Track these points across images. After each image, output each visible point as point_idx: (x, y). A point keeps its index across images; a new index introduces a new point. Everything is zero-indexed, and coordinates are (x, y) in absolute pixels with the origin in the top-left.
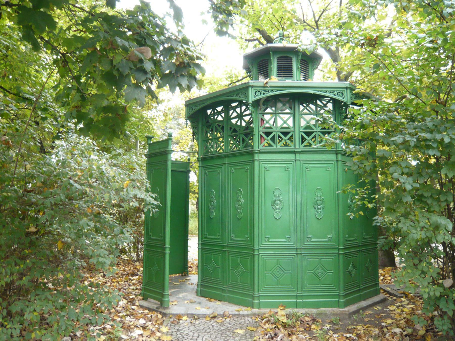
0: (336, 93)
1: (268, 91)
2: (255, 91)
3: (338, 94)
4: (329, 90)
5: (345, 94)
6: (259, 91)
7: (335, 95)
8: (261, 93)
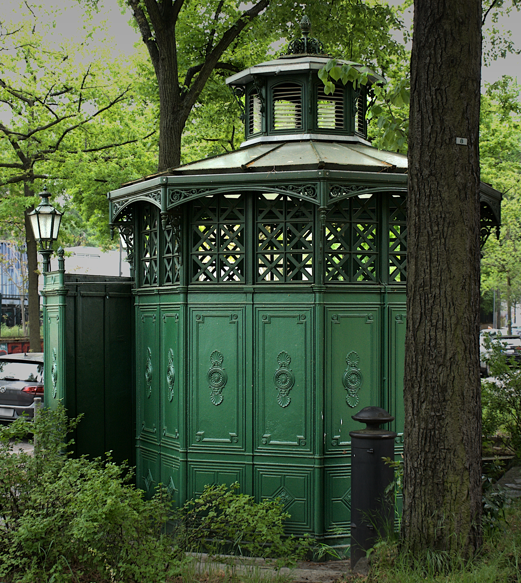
1: (192, 192)
2: (171, 192)
4: (291, 185)
5: (318, 191)
6: (178, 192)
8: (180, 196)
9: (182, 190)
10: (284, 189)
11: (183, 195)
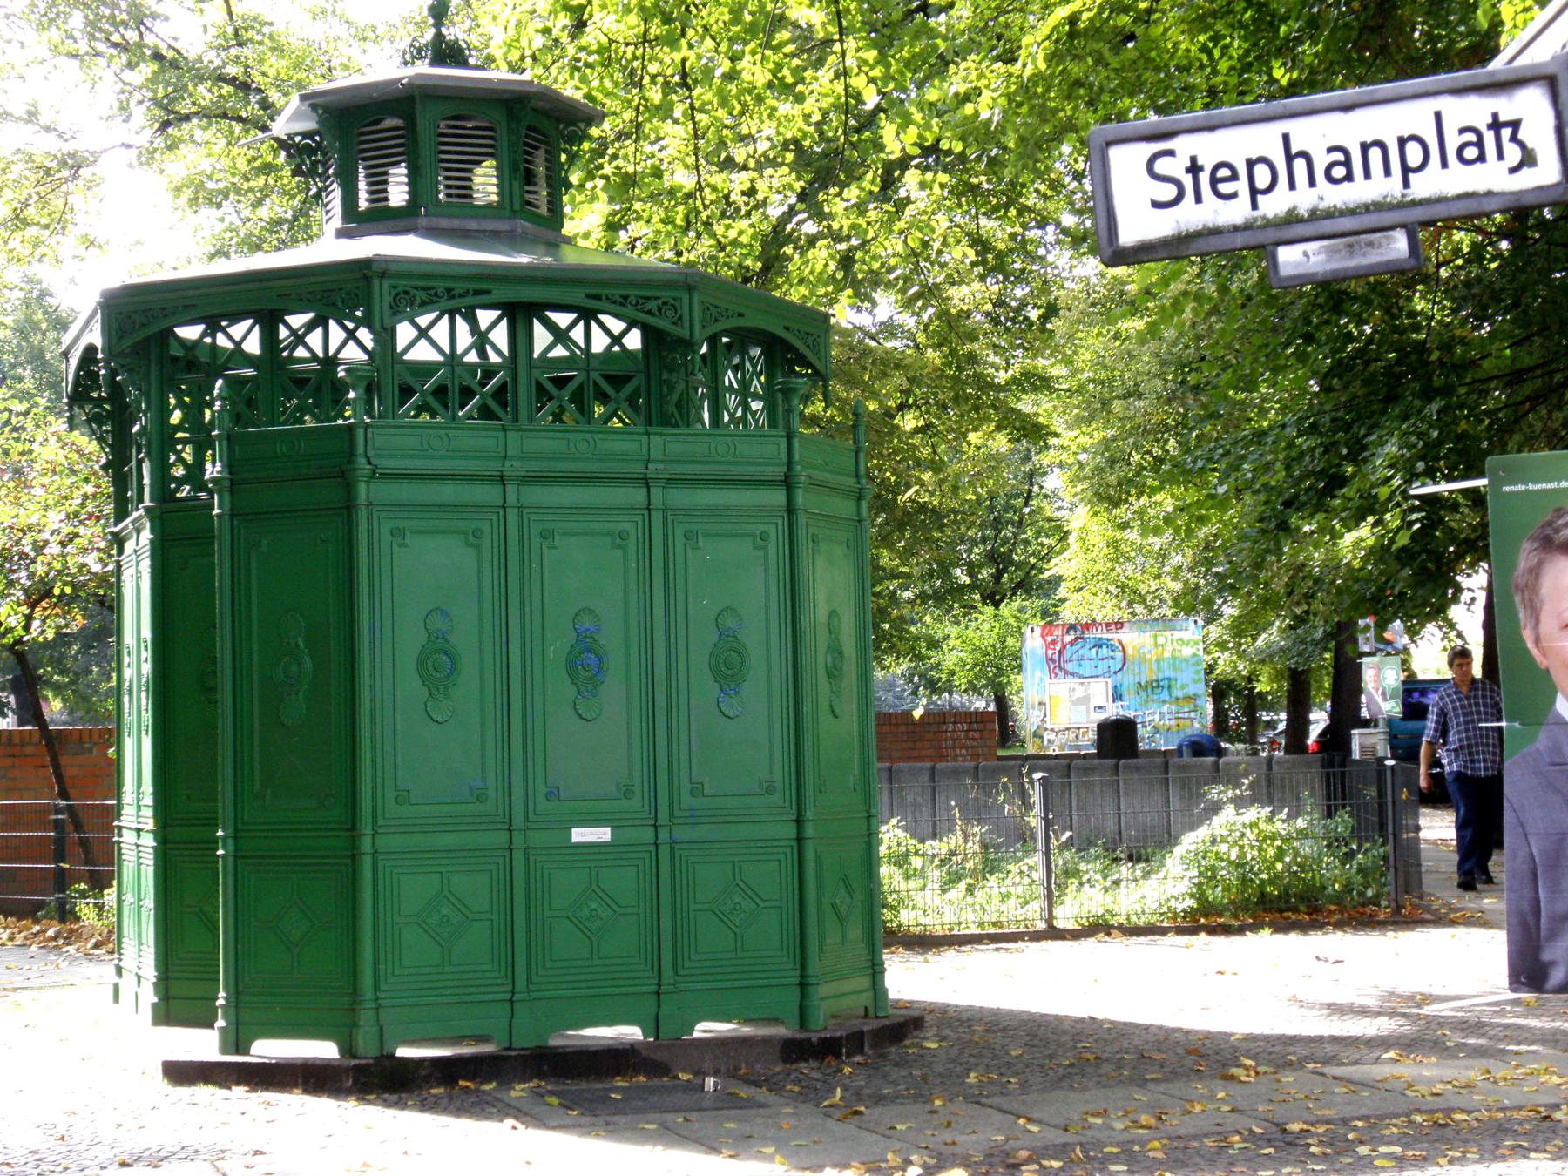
0: (653, 305)
3: (660, 310)
6: (406, 293)
7: (649, 312)
9: (416, 288)
10: (622, 304)
11: (418, 300)
